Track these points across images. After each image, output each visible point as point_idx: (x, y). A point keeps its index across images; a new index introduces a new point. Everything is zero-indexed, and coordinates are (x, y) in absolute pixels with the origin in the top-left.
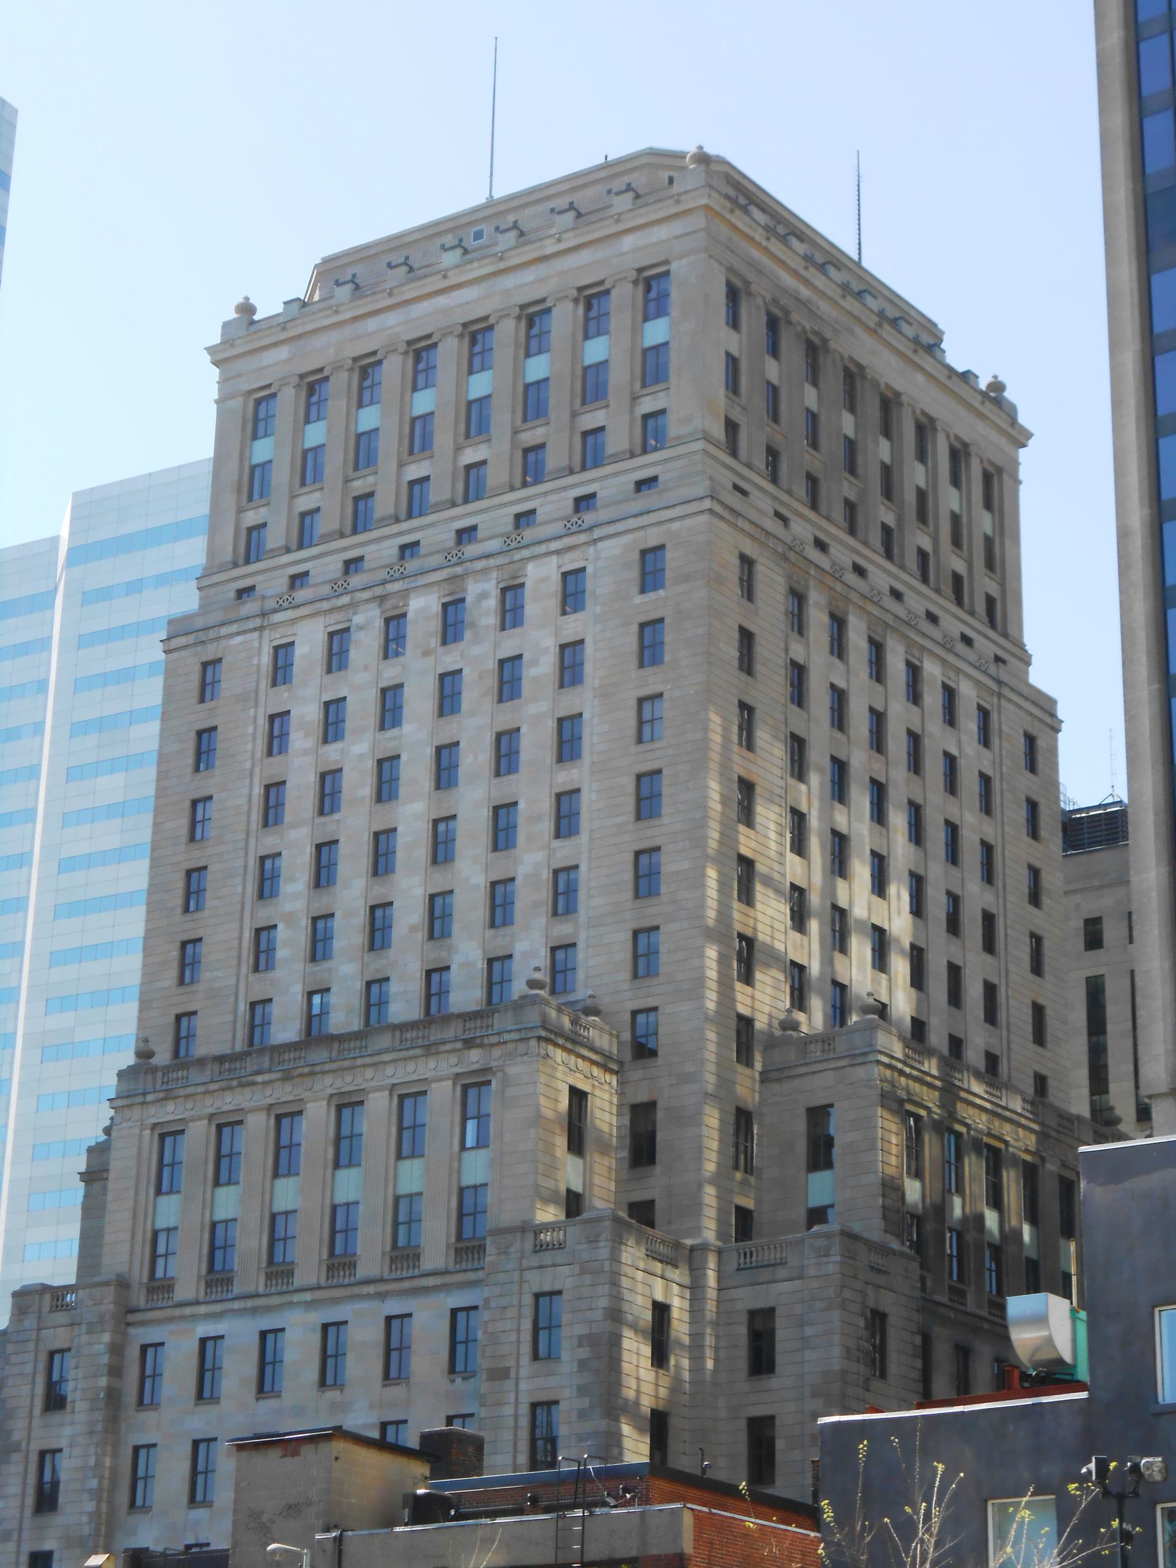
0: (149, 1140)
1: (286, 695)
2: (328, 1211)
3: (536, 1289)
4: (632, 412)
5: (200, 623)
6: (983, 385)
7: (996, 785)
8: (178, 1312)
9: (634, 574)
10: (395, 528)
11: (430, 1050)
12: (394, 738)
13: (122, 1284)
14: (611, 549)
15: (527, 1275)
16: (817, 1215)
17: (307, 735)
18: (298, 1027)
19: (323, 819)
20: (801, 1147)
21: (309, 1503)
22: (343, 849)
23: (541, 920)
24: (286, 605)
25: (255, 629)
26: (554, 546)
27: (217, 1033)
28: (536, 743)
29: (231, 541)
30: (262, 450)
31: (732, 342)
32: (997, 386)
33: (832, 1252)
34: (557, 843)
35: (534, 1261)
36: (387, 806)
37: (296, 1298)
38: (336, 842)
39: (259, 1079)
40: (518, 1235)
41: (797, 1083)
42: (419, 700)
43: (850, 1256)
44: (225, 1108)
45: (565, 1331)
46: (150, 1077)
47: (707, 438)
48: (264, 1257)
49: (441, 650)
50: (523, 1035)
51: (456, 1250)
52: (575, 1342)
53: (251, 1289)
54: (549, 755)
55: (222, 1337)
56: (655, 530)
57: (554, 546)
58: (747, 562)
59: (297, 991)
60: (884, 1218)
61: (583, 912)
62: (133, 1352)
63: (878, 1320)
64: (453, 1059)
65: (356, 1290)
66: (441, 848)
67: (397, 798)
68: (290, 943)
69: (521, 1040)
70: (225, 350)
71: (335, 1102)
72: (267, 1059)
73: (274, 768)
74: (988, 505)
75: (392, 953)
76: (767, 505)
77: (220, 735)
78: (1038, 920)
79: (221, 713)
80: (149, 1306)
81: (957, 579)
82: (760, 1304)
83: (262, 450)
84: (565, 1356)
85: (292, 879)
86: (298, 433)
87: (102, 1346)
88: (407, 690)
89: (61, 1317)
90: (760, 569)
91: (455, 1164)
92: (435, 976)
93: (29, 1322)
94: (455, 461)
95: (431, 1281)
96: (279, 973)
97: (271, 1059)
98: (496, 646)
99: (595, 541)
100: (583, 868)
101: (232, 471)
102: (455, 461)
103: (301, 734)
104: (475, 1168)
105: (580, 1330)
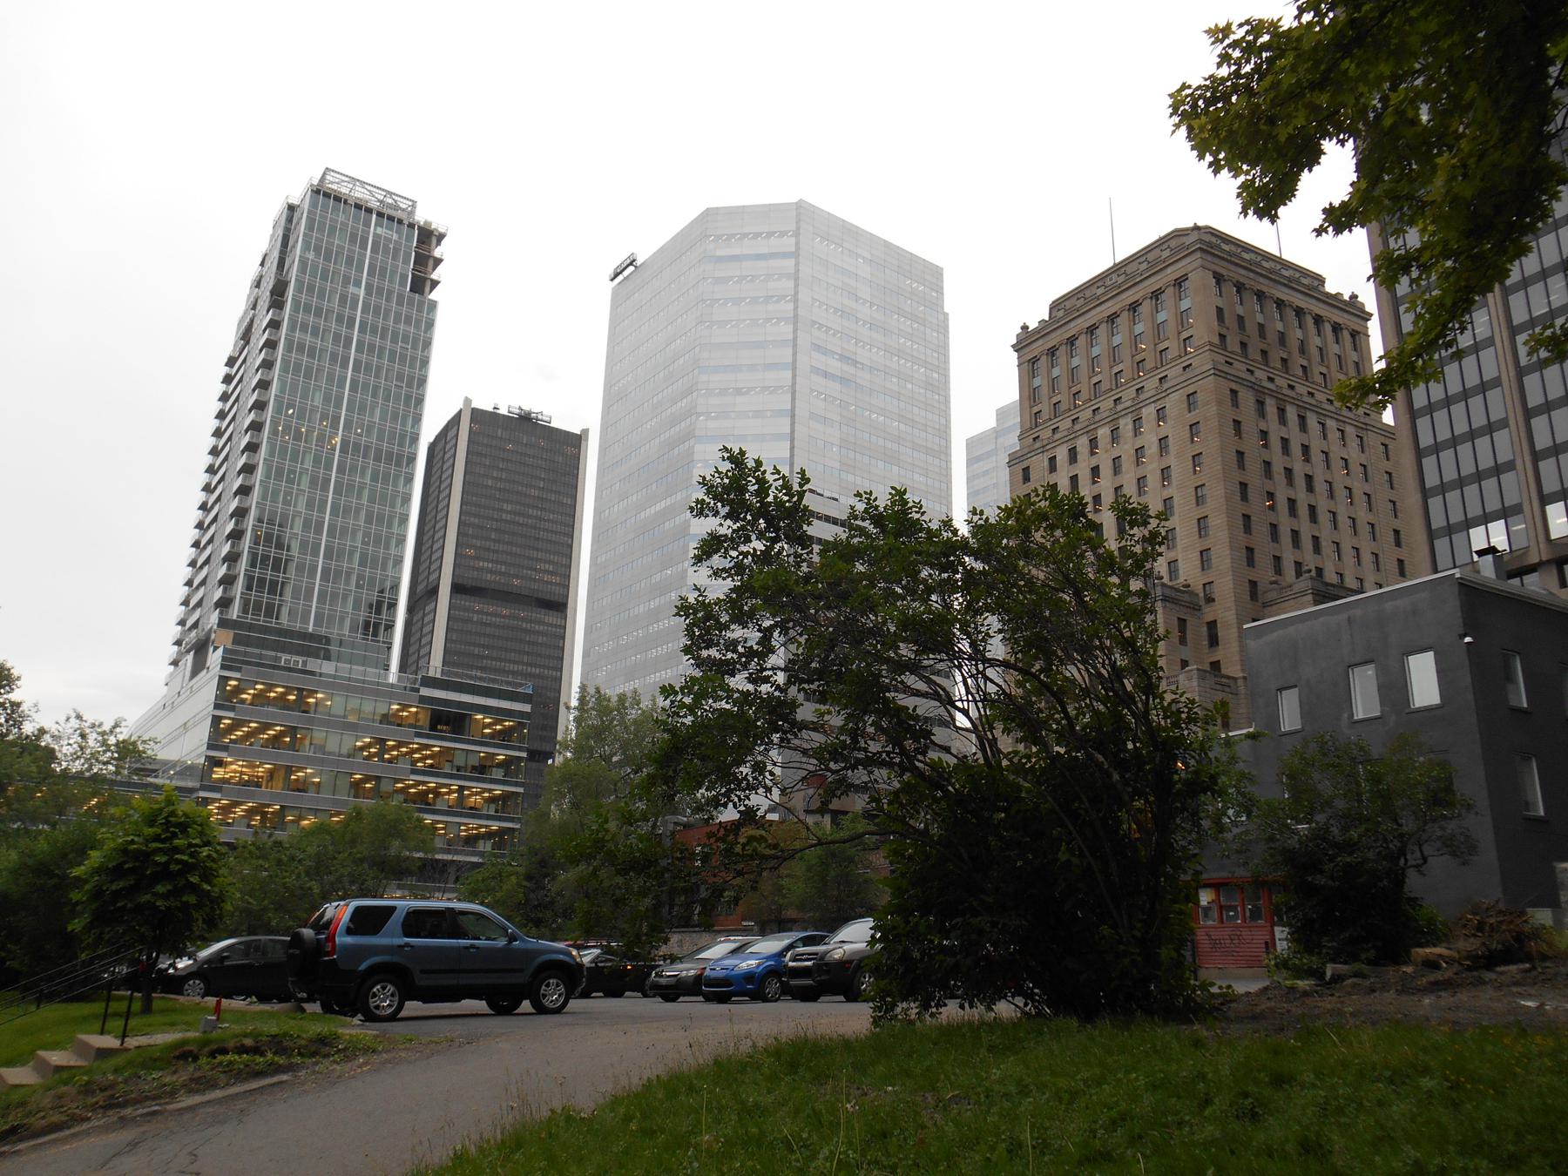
6: (1346, 297)
9: (1185, 405)
14: (1174, 397)
47: (1211, 344)
54: (1159, 485)
58: (1234, 392)
61: (1179, 546)
76: (1243, 367)
83: (1037, 382)
86: (1049, 373)
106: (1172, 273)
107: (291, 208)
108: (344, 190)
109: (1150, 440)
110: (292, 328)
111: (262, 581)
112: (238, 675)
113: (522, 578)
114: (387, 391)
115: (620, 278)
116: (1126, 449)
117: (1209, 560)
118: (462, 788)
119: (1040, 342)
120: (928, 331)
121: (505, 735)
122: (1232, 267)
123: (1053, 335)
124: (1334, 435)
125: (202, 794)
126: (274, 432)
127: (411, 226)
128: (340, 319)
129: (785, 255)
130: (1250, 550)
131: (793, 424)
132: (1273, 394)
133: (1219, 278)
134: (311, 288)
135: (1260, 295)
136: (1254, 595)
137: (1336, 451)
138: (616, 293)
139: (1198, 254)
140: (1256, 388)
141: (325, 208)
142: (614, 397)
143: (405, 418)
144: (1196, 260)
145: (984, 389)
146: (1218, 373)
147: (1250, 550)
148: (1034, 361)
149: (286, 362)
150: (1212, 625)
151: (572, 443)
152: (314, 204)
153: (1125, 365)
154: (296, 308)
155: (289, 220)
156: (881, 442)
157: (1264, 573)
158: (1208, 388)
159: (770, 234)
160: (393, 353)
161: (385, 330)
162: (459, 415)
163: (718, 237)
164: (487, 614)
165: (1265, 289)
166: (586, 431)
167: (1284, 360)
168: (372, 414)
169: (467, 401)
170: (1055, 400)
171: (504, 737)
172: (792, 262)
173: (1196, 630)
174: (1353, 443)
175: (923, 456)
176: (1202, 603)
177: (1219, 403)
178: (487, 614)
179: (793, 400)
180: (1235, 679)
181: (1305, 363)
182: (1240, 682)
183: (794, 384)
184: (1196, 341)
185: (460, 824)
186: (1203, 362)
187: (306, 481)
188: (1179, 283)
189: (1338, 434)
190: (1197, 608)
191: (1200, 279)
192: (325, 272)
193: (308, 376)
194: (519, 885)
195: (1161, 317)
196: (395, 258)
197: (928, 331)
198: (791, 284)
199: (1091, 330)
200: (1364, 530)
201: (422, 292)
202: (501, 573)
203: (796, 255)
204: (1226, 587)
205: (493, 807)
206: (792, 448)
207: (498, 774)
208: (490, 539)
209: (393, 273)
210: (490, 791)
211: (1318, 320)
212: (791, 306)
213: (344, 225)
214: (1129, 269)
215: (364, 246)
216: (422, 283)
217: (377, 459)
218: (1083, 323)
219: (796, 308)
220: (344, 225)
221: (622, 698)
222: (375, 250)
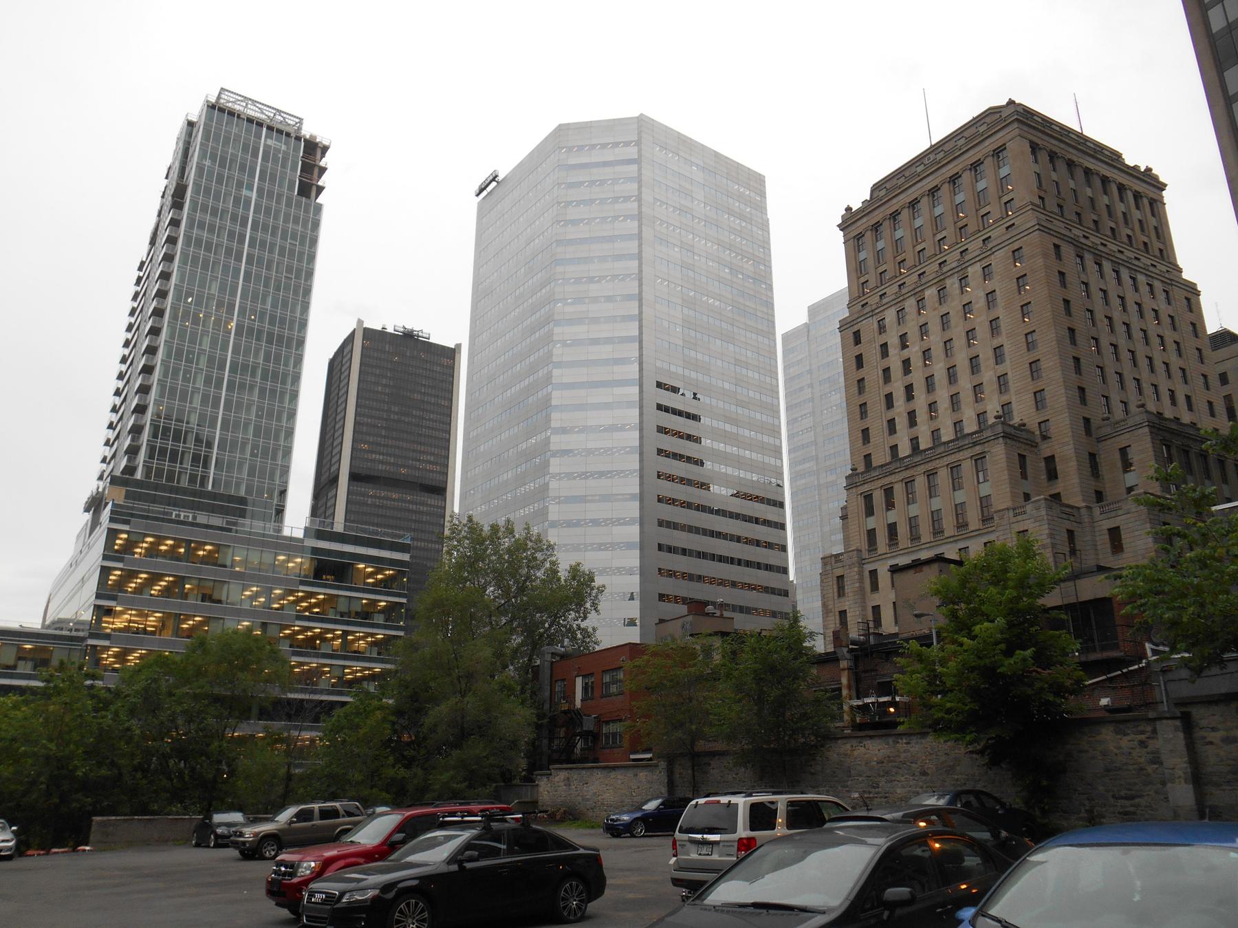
7: (1176, 319)
11: (960, 449)
13: (859, 551)
16: (1130, 490)
20: (1119, 464)
23: (996, 396)
27: (881, 457)
28: (982, 330)
30: (862, 255)
31: (1037, 168)
32: (1148, 170)
35: (1014, 520)
42: (935, 326)
47: (1032, 204)
54: (989, 335)
58: (1057, 247)
62: (867, 574)
74: (1153, 215)
78: (1204, 369)
81: (1145, 244)
83: (862, 255)
86: (874, 246)
89: (839, 564)
92: (958, 424)
93: (828, 567)
96: (898, 434)
104: (985, 490)
106: (990, 145)
107: (191, 124)
108: (237, 107)
109: (976, 292)
110: (191, 225)
111: (163, 452)
112: (126, 528)
113: (408, 467)
114: (278, 282)
115: (485, 193)
116: (954, 306)
117: (1043, 399)
118: (346, 633)
119: (865, 220)
120: (754, 229)
121: (386, 584)
122: (1046, 138)
123: (876, 213)
124: (1144, 289)
125: (91, 642)
126: (174, 317)
127: (298, 138)
128: (234, 218)
129: (629, 162)
130: (1082, 390)
131: (640, 306)
132: (1091, 249)
133: (1034, 148)
134: (207, 191)
136: (1088, 431)
137: (1148, 304)
138: (481, 207)
139: (1016, 125)
140: (1073, 242)
141: (219, 122)
142: (482, 294)
143: (294, 305)
144: (1014, 129)
145: (809, 272)
146: (1043, 229)
147: (1082, 390)
148: (859, 237)
149: (185, 255)
150: (1050, 460)
151: (449, 355)
152: (209, 118)
153: (949, 232)
154: (194, 208)
155: (190, 134)
156: (718, 323)
157: (1096, 411)
158: (1034, 244)
159: (616, 145)
160: (282, 249)
161: (275, 228)
162: (353, 334)
163: (570, 149)
164: (379, 498)
165: (1075, 159)
166: (459, 346)
167: (1095, 222)
168: (264, 302)
169: (360, 322)
170: (881, 269)
171: (385, 586)
172: (634, 167)
173: (1036, 467)
174: (1161, 297)
175: (754, 336)
176: (1038, 440)
177: (1045, 256)
178: (379, 498)
179: (640, 285)
180: (1078, 508)
181: (1113, 225)
182: (1083, 511)
183: (641, 271)
184: (1017, 204)
185: (345, 667)
186: (1028, 220)
187: (203, 363)
188: (998, 152)
189: (1147, 288)
191: (1017, 147)
192: (220, 177)
193: (205, 267)
194: (384, 720)
195: (981, 185)
196: (284, 166)
197: (754, 229)
198: (635, 186)
199: (913, 204)
200: (1177, 374)
201: (308, 197)
202: (390, 464)
203: (637, 161)
205: (375, 649)
206: (641, 327)
207: (379, 619)
208: (381, 436)
209: (282, 179)
210: (372, 635)
211: (1121, 188)
212: (636, 205)
213: (238, 137)
214: (946, 148)
215: (255, 155)
216: (309, 187)
217: (270, 342)
218: (905, 198)
219: (640, 206)
220: (238, 137)
221: (495, 528)
222: (265, 158)
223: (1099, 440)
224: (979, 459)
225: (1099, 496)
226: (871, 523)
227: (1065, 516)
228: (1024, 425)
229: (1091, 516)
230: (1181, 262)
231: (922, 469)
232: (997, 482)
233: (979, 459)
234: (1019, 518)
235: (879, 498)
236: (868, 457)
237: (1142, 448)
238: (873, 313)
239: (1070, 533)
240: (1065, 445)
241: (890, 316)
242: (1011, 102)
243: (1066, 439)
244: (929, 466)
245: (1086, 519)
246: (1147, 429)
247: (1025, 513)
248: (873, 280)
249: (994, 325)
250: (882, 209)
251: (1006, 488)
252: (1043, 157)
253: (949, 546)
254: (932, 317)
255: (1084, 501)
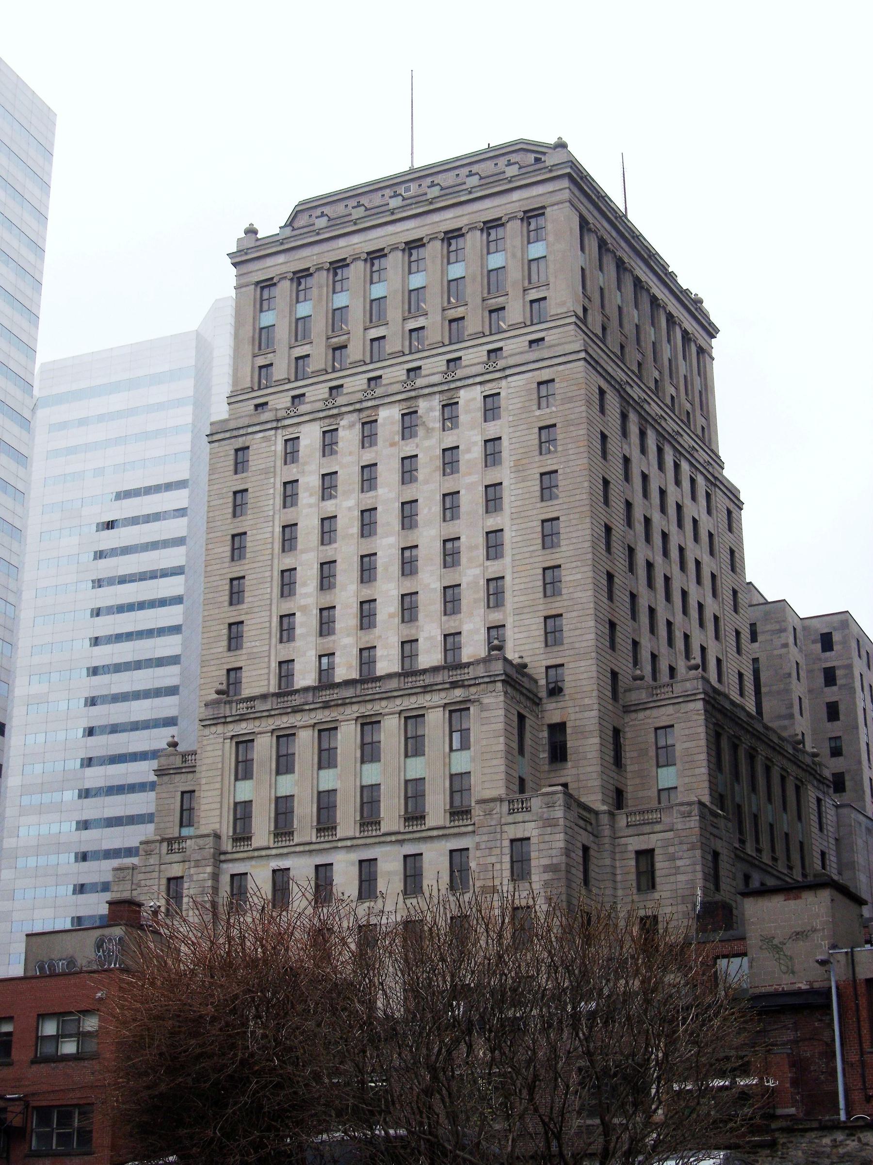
0: (229, 748)
1: (295, 470)
2: (358, 790)
3: (512, 837)
4: (524, 299)
5: (233, 425)
8: (256, 854)
10: (364, 368)
12: (372, 497)
15: (505, 828)
17: (311, 495)
18: (313, 677)
19: (324, 548)
21: (815, 930)
22: (340, 567)
23: (481, 610)
24: (292, 414)
25: (272, 429)
26: (478, 379)
27: (258, 680)
28: (471, 500)
29: (249, 374)
30: (267, 319)
33: (693, 814)
34: (489, 563)
35: (510, 819)
36: (369, 539)
37: (340, 844)
38: (335, 561)
39: (307, 707)
40: (498, 803)
41: (648, 712)
42: (388, 474)
43: (702, 817)
44: (282, 726)
45: (534, 863)
46: (227, 706)
48: (315, 819)
49: (402, 443)
50: (492, 679)
51: (450, 813)
52: (542, 870)
53: (307, 839)
54: (481, 510)
55: (289, 869)
56: (547, 370)
57: (478, 379)
58: (602, 392)
59: (394, 641)
60: (710, 795)
62: (225, 879)
63: (716, 855)
64: (443, 694)
65: (383, 839)
66: (408, 564)
67: (375, 534)
68: (306, 624)
69: (491, 682)
70: (241, 256)
71: (360, 721)
72: (311, 694)
73: (289, 516)
75: (377, 631)
77: (250, 495)
79: (250, 480)
80: (234, 850)
82: (644, 847)
83: (267, 319)
84: (535, 878)
85: (304, 584)
87: (206, 875)
88: (380, 467)
90: (607, 396)
91: (447, 760)
92: (408, 646)
94: (403, 328)
95: (435, 833)
96: (298, 643)
97: (314, 695)
98: (441, 441)
99: (506, 377)
100: (508, 579)
101: (248, 331)
102: (403, 328)
103: (307, 494)
104: (461, 762)
105: (546, 861)
106: (518, 201)
109: (470, 437)
116: (428, 447)
119: (281, 259)
133: (584, 224)
135: (621, 265)
146: (592, 362)
148: (267, 284)
150: (558, 730)
170: (299, 352)
176: (543, 694)
177: (589, 403)
180: (597, 813)
182: (605, 819)
186: (565, 339)
190: (536, 702)
204: (583, 676)
223: (627, 710)
224: (457, 711)
225: (619, 798)
226: (245, 791)
227: (582, 823)
228: (525, 666)
229: (613, 827)
230: (724, 452)
231: (354, 711)
232: (486, 757)
233: (457, 711)
234: (519, 817)
235: (264, 749)
236: (234, 672)
237: (690, 732)
238: (277, 424)
239: (586, 849)
240: (582, 708)
241: (310, 436)
242: (561, 145)
243: (587, 701)
244: (367, 709)
245: (607, 832)
246: (700, 705)
247: (528, 810)
248: (281, 369)
249: (493, 496)
250: (316, 249)
251: (499, 765)
252: (592, 243)
253: (387, 848)
254: (387, 457)
255: (604, 802)
